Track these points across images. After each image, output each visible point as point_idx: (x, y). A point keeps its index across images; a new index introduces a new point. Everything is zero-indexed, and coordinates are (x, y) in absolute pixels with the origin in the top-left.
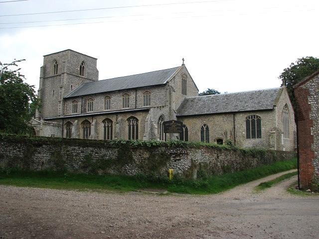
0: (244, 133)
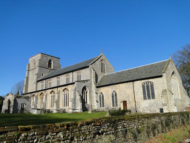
0: (141, 95)
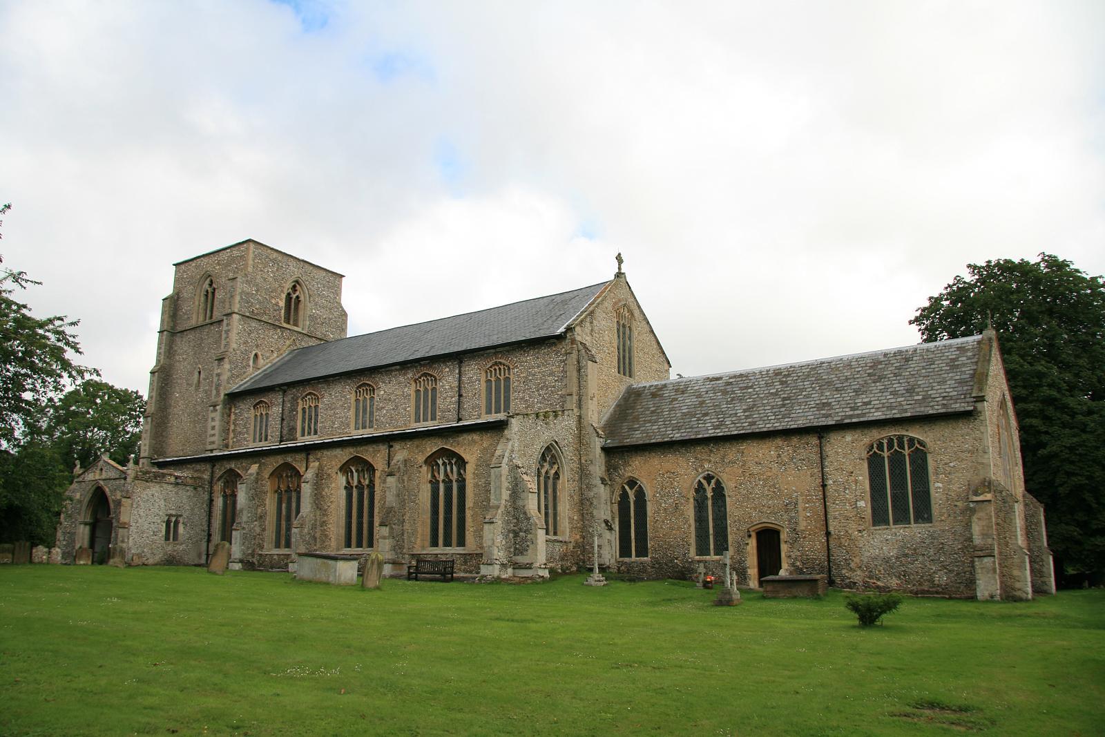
0: (861, 504)
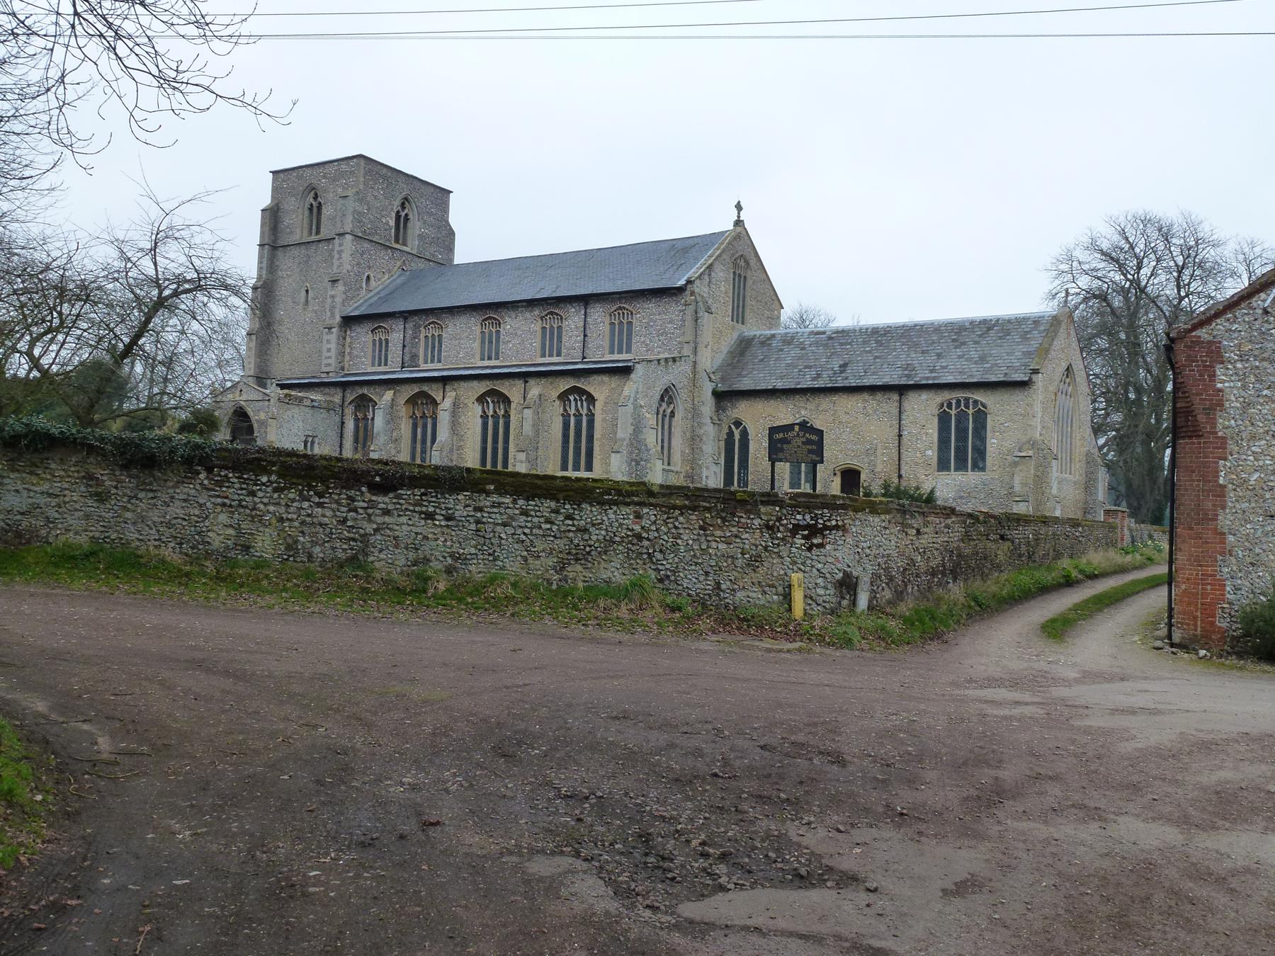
0: (929, 453)
